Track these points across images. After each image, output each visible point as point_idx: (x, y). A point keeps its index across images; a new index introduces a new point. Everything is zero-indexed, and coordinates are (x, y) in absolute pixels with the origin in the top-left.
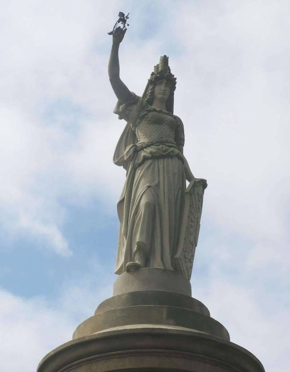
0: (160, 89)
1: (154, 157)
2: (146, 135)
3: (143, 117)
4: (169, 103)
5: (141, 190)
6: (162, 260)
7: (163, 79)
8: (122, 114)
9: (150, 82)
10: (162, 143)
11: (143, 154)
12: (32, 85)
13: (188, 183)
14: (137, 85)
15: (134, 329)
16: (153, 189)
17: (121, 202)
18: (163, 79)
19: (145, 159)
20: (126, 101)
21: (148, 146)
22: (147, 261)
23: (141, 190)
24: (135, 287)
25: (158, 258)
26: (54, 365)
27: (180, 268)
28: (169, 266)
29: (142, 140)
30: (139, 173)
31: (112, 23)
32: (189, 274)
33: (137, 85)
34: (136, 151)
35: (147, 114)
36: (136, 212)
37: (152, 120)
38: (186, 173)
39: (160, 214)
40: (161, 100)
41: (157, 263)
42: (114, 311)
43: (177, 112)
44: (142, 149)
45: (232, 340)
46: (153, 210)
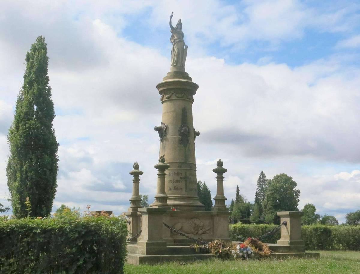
0: (179, 26)
1: (178, 42)
2: (176, 36)
3: (176, 33)
5: (176, 50)
6: (180, 63)
7: (180, 24)
9: (177, 25)
11: (176, 41)
13: (185, 47)
16: (178, 49)
17: (172, 51)
18: (180, 24)
19: (176, 42)
21: (177, 39)
23: (176, 50)
24: (175, 71)
25: (179, 63)
28: (182, 66)
29: (176, 38)
31: (171, 14)
32: (183, 62)
33: (174, 25)
34: (175, 40)
35: (77, 238)
36: (175, 54)
37: (238, 188)
38: (184, 44)
42: (171, 76)
43: (182, 30)
44: (176, 40)
45: (189, 76)
46: (178, 54)
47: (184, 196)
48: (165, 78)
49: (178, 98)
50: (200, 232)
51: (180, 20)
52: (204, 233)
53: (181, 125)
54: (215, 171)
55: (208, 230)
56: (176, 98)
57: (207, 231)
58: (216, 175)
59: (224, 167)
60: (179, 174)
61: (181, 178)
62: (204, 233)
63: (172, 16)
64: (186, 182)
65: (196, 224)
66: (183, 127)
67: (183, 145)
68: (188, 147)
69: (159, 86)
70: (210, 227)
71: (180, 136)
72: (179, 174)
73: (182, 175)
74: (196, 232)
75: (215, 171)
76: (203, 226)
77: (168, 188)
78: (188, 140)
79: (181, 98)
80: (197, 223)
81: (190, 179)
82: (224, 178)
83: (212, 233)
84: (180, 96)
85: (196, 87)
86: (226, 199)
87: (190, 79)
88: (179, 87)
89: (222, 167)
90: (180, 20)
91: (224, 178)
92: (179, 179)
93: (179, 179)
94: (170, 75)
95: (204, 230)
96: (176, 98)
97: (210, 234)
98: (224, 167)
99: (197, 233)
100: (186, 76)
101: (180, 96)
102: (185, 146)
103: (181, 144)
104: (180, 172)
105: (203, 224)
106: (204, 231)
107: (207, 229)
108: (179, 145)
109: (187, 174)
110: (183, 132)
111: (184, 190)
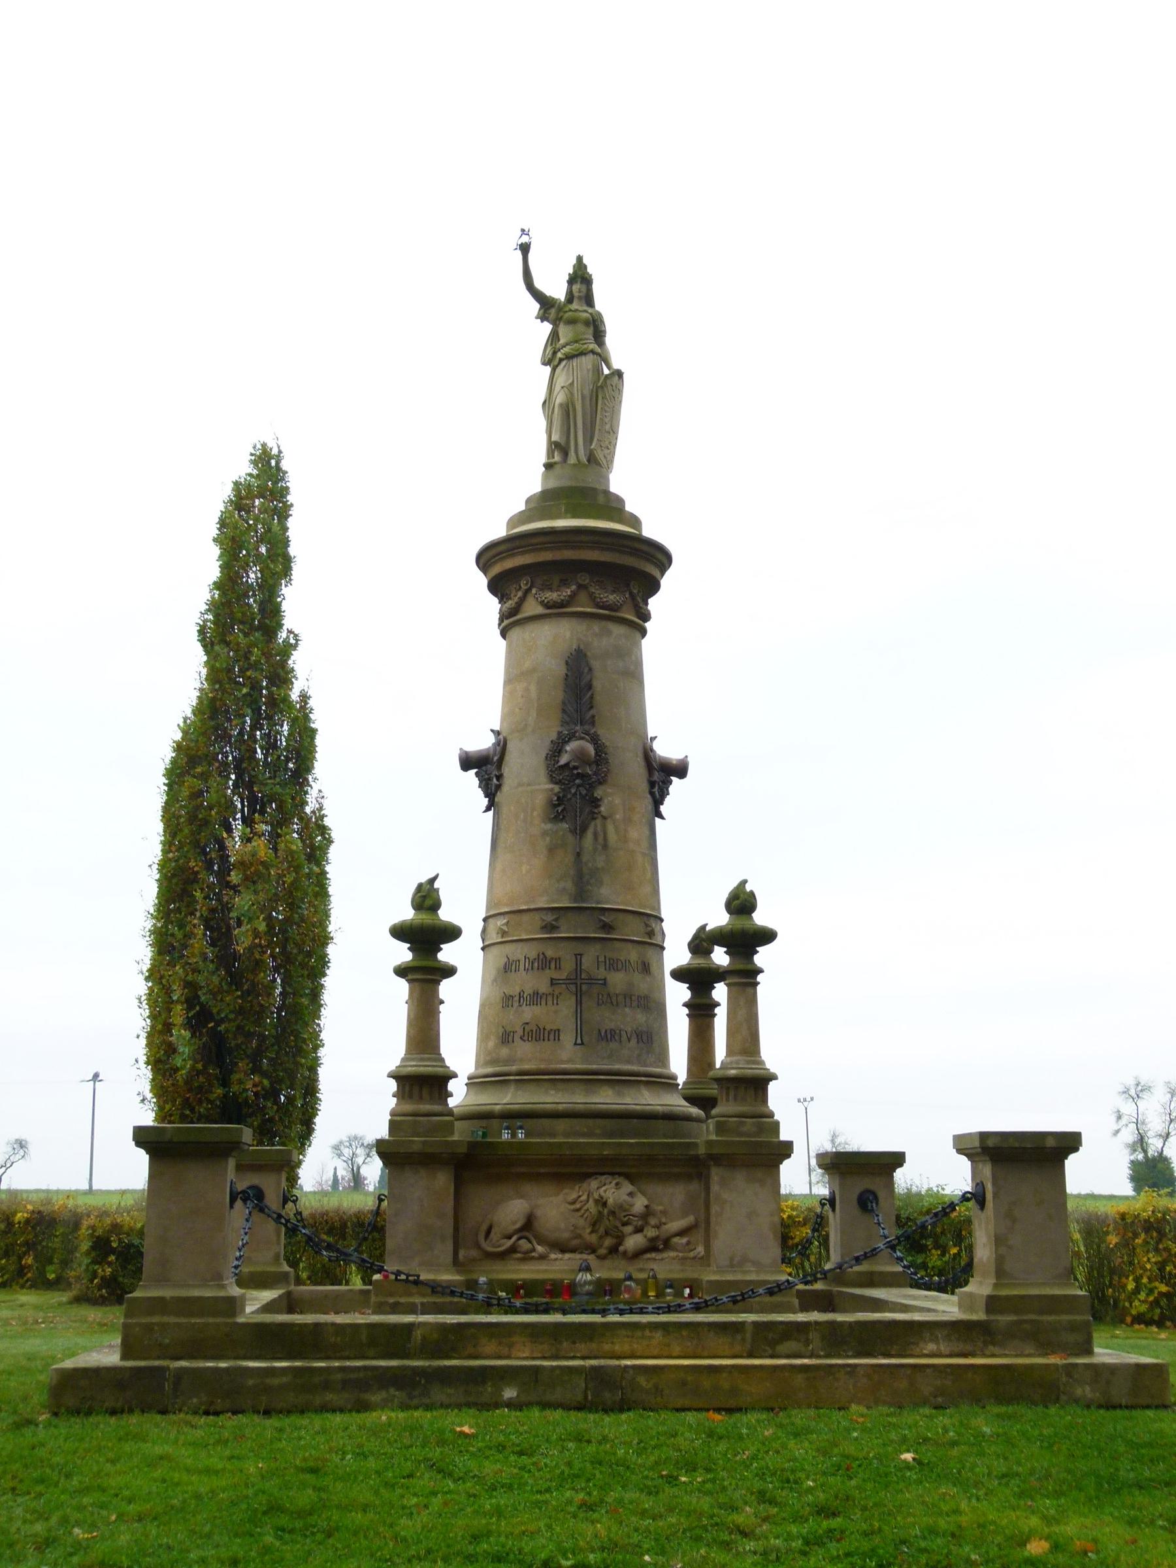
4: (589, 300)
7: (580, 278)
8: (543, 317)
10: (576, 342)
12: (96, 1077)
14: (557, 290)
15: (282, 676)
17: (544, 403)
18: (580, 278)
19: (561, 360)
20: (546, 305)
21: (567, 344)
22: (565, 453)
24: (553, 484)
26: (494, 551)
27: (597, 460)
30: (558, 370)
31: (515, 239)
33: (557, 290)
39: (574, 410)
40: (580, 298)
41: (572, 459)
47: (526, 1067)
48: (514, 521)
49: (549, 608)
50: (633, 1242)
51: (580, 259)
52: (653, 1247)
53: (559, 733)
54: (400, 932)
55: (681, 1233)
56: (540, 610)
57: (676, 1240)
58: (403, 953)
59: (761, 918)
60: (543, 963)
61: (553, 982)
62: (653, 1247)
63: (525, 249)
64: (579, 1003)
65: (605, 1204)
66: (572, 737)
67: (565, 826)
68: (595, 835)
69: (494, 551)
70: (690, 1219)
71: (556, 783)
72: (543, 963)
73: (558, 968)
74: (608, 1242)
75: (400, 932)
76: (648, 1212)
77: (501, 1030)
78: (595, 802)
79: (562, 605)
80: (610, 1201)
81: (605, 984)
82: (761, 971)
83: (700, 1250)
84: (553, 596)
85: (660, 557)
86: (774, 1077)
87: (635, 521)
88: (547, 556)
89: (752, 918)
90: (580, 259)
91: (761, 971)
92: (544, 988)
93: (544, 988)
94: (543, 503)
95: (651, 1233)
96: (540, 610)
97: (692, 1254)
98: (761, 918)
99: (614, 1250)
100: (613, 507)
101: (553, 596)
102: (580, 831)
103: (557, 818)
104: (550, 953)
105: (646, 1202)
106: (652, 1240)
107: (675, 1225)
108: (549, 826)
109: (587, 962)
110: (567, 765)
111: (568, 1038)
